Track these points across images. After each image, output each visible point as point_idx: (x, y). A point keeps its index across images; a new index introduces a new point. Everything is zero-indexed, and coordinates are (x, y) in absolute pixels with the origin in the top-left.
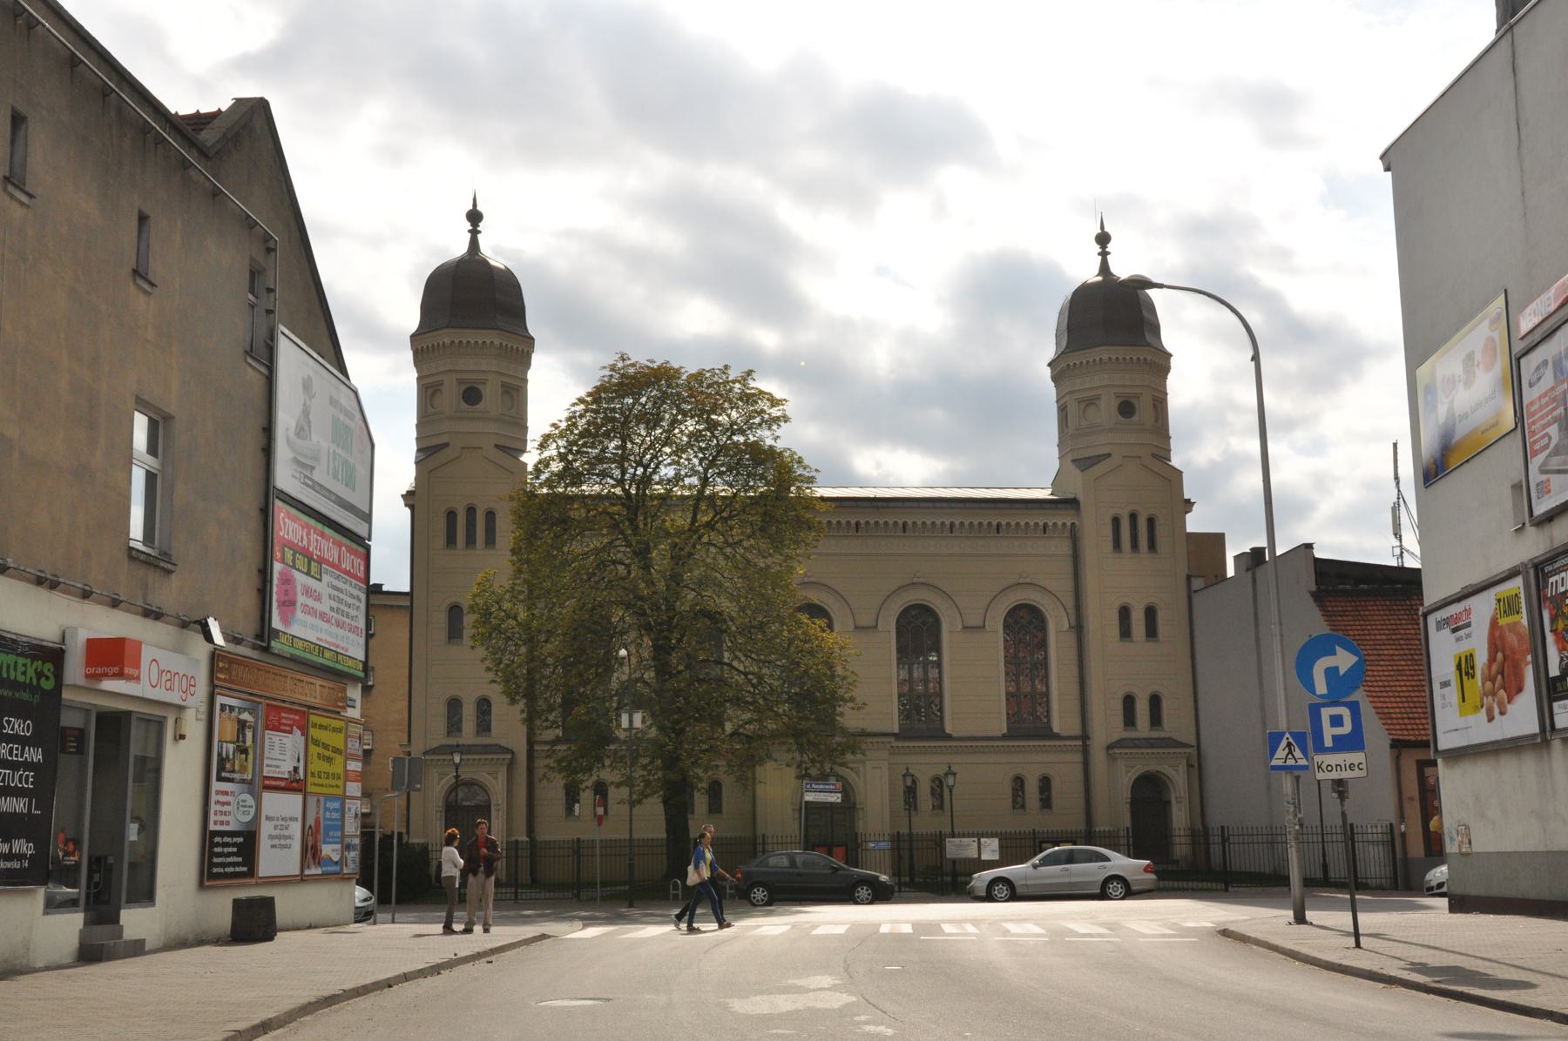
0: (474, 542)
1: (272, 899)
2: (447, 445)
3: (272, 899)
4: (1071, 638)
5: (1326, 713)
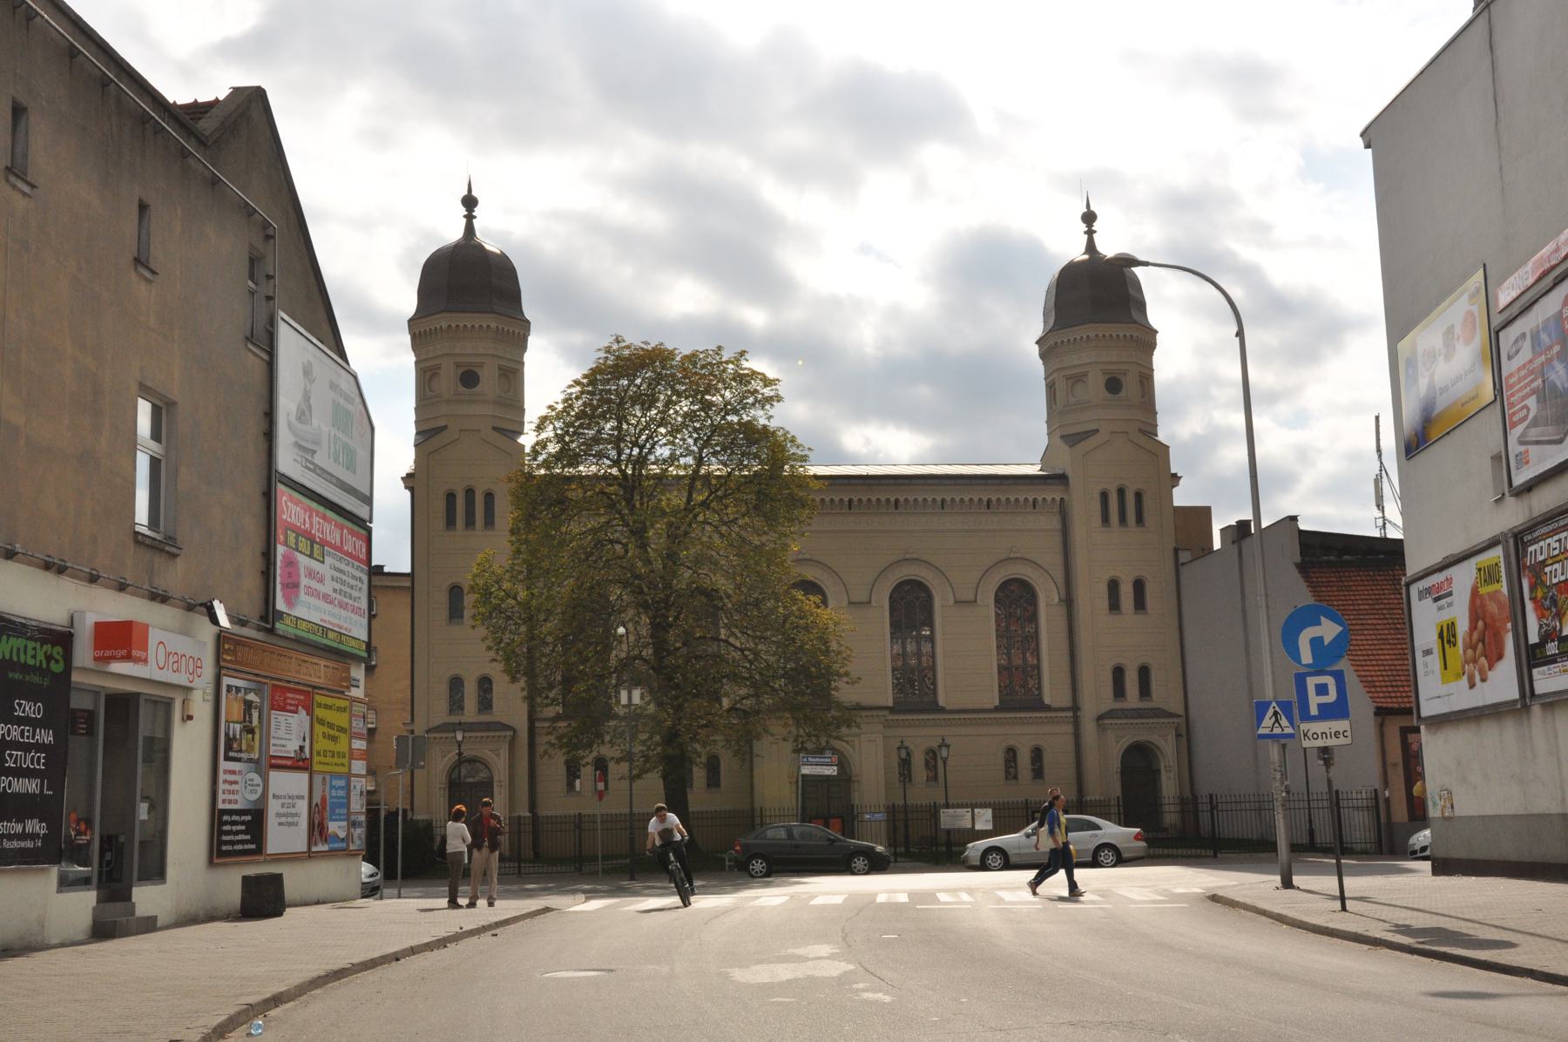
0: (474, 523)
2: (445, 427)
4: (1061, 611)
5: (1311, 682)
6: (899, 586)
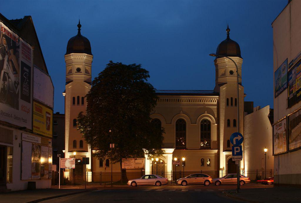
0: (79, 104)
1: (35, 182)
3: (35, 182)
5: (235, 148)
6: (177, 122)
